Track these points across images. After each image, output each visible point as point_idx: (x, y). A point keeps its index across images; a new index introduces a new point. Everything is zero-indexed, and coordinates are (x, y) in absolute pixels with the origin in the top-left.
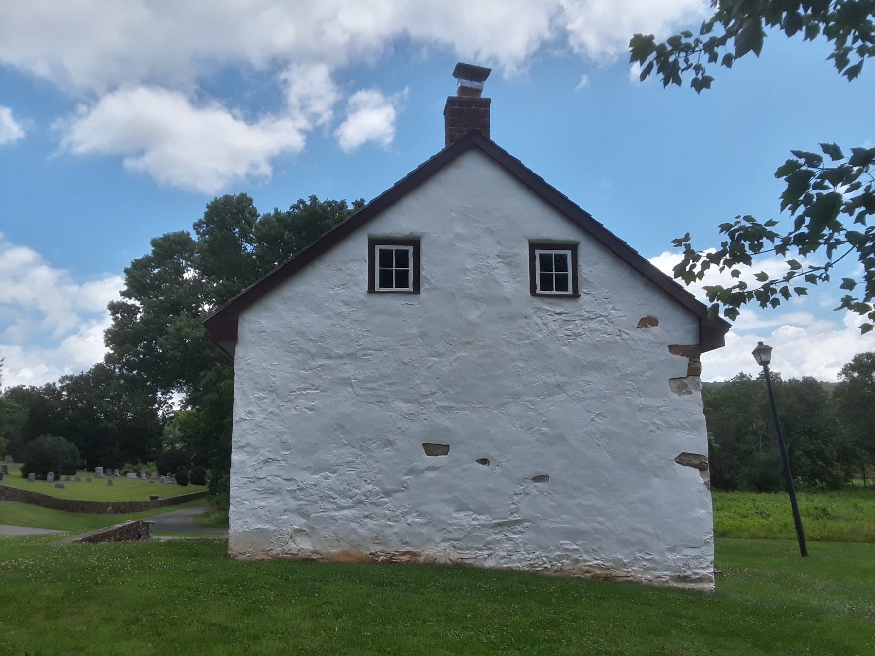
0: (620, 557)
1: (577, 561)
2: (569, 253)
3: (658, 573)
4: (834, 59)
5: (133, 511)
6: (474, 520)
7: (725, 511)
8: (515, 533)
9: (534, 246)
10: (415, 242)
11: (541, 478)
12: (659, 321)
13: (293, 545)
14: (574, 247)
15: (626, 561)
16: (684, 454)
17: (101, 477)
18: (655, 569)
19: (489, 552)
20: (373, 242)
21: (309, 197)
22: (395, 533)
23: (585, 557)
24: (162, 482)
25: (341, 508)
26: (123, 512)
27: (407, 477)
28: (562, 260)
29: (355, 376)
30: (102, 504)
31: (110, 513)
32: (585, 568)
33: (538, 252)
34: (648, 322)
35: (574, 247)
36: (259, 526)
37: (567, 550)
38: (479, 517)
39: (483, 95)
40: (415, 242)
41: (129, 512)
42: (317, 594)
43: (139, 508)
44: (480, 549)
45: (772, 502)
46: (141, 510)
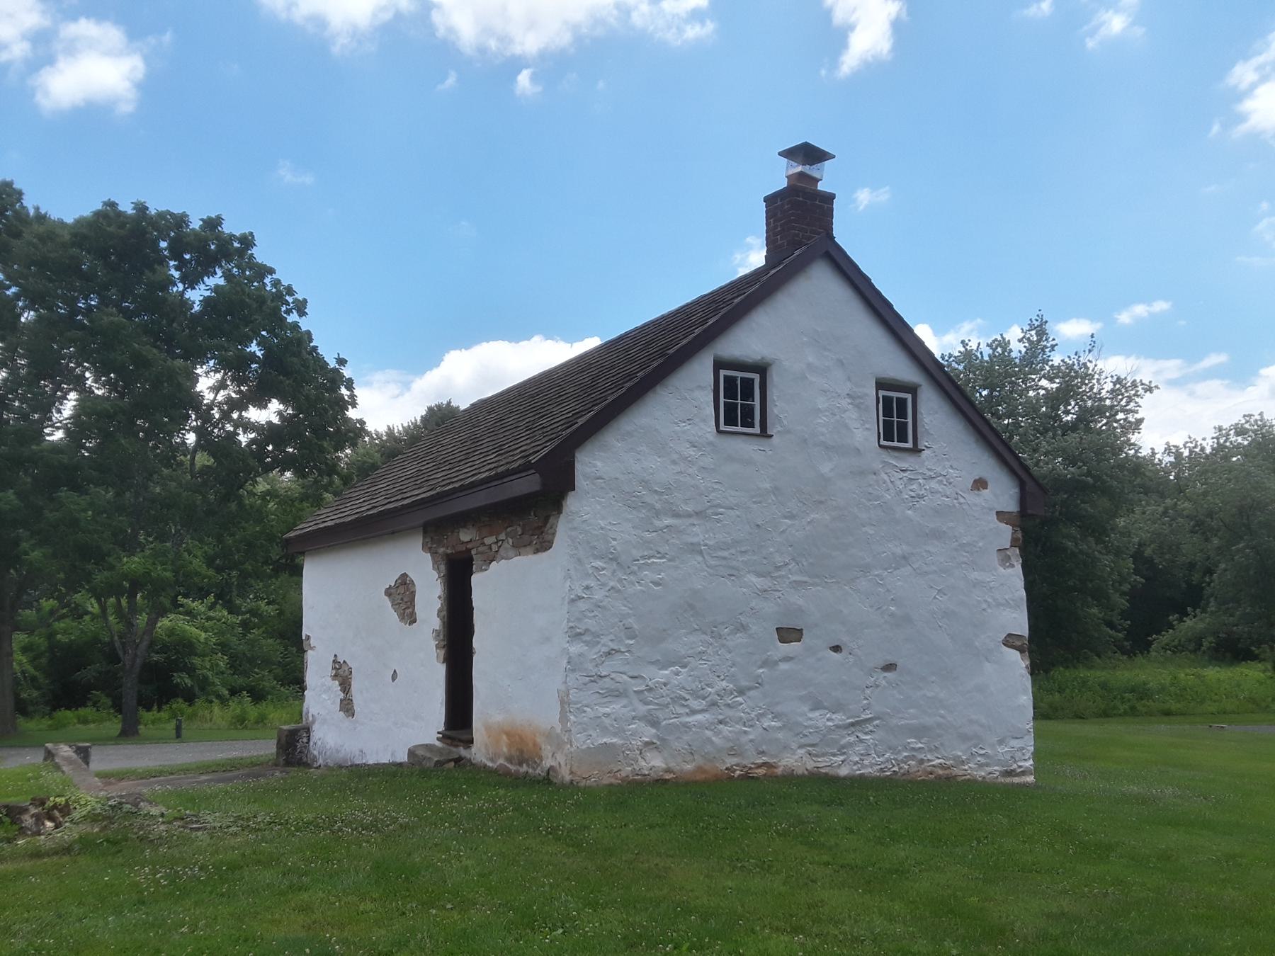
0: (960, 754)
1: (921, 762)
2: (757, 377)
3: (989, 769)
8: (866, 734)
9: (881, 385)
11: (890, 667)
12: (989, 483)
16: (1010, 635)
18: (987, 765)
19: (842, 758)
20: (719, 365)
22: (751, 741)
23: (929, 757)
25: (694, 712)
27: (761, 671)
28: (748, 384)
32: (929, 769)
33: (722, 373)
34: (980, 484)
35: (913, 389)
36: (605, 740)
37: (913, 749)
38: (834, 717)
40: (762, 369)
44: (834, 755)
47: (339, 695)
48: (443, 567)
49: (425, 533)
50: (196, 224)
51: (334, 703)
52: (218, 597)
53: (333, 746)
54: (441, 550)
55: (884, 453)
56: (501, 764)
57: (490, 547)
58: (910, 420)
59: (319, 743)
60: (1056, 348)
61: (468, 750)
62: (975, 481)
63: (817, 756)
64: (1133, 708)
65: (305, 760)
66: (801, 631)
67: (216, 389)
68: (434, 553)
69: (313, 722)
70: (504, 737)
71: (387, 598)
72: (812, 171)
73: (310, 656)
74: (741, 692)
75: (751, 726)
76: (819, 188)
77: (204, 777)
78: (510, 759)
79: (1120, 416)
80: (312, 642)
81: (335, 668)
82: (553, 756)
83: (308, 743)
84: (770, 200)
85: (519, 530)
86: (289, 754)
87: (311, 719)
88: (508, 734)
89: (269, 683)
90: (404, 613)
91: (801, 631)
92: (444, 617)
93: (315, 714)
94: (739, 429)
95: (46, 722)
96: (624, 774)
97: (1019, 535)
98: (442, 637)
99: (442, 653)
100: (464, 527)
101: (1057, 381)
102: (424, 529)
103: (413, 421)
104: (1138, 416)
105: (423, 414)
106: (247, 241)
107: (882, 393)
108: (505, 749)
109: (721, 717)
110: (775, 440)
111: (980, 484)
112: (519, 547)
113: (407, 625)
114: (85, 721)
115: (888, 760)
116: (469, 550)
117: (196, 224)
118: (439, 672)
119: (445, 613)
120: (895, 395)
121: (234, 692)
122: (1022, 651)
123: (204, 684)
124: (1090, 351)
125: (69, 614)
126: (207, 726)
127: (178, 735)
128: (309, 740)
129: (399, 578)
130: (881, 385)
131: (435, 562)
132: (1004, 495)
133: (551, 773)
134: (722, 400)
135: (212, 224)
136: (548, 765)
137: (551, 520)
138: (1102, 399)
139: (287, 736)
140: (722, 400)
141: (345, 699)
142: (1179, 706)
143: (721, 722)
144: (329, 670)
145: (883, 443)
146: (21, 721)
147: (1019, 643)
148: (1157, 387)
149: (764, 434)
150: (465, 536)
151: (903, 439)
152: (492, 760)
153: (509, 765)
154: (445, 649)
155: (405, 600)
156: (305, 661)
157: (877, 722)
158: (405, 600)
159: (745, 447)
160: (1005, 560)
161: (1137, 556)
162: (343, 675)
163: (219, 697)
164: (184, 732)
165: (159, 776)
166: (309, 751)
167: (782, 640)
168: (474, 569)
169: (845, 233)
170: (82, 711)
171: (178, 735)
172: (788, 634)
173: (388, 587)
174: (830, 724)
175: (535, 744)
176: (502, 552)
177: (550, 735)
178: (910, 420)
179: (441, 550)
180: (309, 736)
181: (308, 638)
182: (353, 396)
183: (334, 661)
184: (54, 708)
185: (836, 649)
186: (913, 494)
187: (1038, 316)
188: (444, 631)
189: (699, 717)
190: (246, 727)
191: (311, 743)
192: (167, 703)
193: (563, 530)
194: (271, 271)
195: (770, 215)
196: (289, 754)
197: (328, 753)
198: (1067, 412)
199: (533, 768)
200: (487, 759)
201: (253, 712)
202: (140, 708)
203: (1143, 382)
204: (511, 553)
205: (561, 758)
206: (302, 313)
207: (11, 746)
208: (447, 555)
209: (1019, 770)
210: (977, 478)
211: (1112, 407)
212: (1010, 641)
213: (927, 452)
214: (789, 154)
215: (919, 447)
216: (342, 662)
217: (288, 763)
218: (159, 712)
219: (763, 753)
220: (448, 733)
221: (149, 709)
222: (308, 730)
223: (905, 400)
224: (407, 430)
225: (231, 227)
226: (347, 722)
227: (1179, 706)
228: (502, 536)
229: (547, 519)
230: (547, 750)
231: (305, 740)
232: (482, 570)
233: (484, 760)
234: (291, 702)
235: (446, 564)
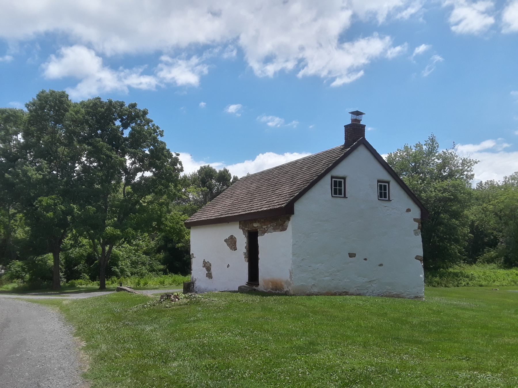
0: (401, 291)
1: (390, 293)
2: (343, 180)
3: (410, 296)
6: (363, 280)
8: (374, 284)
9: (379, 181)
10: (344, 178)
11: (381, 265)
12: (411, 209)
13: (312, 290)
14: (388, 182)
15: (403, 292)
16: (417, 256)
18: (410, 294)
19: (367, 291)
20: (332, 177)
21: (419, 142)
22: (341, 285)
23: (392, 291)
25: (326, 276)
27: (344, 265)
28: (340, 183)
32: (392, 295)
33: (333, 180)
34: (408, 210)
35: (388, 182)
36: (302, 283)
37: (388, 289)
38: (365, 279)
39: (361, 123)
40: (344, 178)
42: (202, 104)
44: (365, 290)
48: (247, 234)
50: (127, 105)
52: (125, 239)
54: (246, 229)
55: (379, 201)
56: (269, 291)
57: (265, 229)
58: (387, 191)
59: (198, 287)
60: (439, 146)
61: (257, 287)
62: (407, 209)
63: (360, 290)
64: (468, 284)
66: (355, 254)
67: (132, 164)
68: (243, 230)
70: (270, 283)
71: (225, 242)
72: (358, 117)
73: (194, 261)
74: (338, 271)
75: (341, 281)
76: (361, 123)
78: (272, 289)
79: (465, 173)
82: (287, 287)
83: (193, 287)
84: (346, 127)
85: (275, 224)
87: (194, 280)
88: (272, 282)
91: (355, 254)
93: (196, 278)
94: (338, 196)
96: (307, 293)
97: (421, 226)
98: (247, 254)
99: (247, 259)
100: (255, 222)
101: (441, 159)
103: (194, 172)
104: (472, 173)
105: (199, 170)
106: (145, 113)
107: (379, 184)
108: (271, 287)
109: (333, 278)
110: (348, 198)
111: (408, 210)
112: (275, 229)
115: (380, 292)
116: (257, 229)
117: (127, 105)
118: (245, 265)
119: (247, 247)
120: (383, 184)
121: (132, 274)
122: (421, 261)
123: (122, 271)
124: (453, 148)
130: (379, 181)
131: (244, 232)
132: (416, 212)
133: (287, 292)
134: (333, 187)
135: (133, 106)
136: (286, 290)
137: (286, 222)
138: (458, 167)
140: (333, 187)
141: (208, 273)
142: (485, 283)
143: (333, 280)
144: (202, 264)
145: (379, 198)
147: (420, 258)
148: (479, 161)
149: (345, 197)
150: (255, 225)
151: (385, 197)
152: (266, 290)
153: (272, 291)
155: (232, 243)
157: (377, 281)
158: (232, 243)
159: (340, 201)
160: (416, 234)
161: (472, 226)
162: (207, 266)
163: (128, 276)
166: (194, 290)
167: (350, 257)
168: (259, 234)
169: (369, 136)
172: (352, 255)
174: (364, 281)
175: (281, 285)
176: (269, 230)
177: (287, 282)
178: (387, 191)
179: (246, 229)
181: (193, 254)
182: (182, 168)
185: (365, 259)
186: (388, 214)
187: (432, 135)
189: (327, 278)
191: (195, 287)
192: (110, 278)
193: (290, 225)
194: (152, 121)
195: (346, 131)
197: (202, 290)
198: (445, 172)
199: (281, 291)
200: (264, 290)
203: (474, 160)
204: (272, 231)
205: (290, 288)
206: (162, 136)
208: (248, 230)
209: (419, 296)
210: (408, 208)
211: (462, 170)
212: (417, 258)
213: (393, 201)
214: (353, 113)
215: (390, 200)
219: (344, 288)
220: (250, 282)
223: (386, 185)
224: (191, 176)
225: (140, 107)
227: (485, 283)
228: (269, 226)
229: (285, 222)
230: (285, 286)
231: (192, 286)
232: (262, 235)
233: (263, 290)
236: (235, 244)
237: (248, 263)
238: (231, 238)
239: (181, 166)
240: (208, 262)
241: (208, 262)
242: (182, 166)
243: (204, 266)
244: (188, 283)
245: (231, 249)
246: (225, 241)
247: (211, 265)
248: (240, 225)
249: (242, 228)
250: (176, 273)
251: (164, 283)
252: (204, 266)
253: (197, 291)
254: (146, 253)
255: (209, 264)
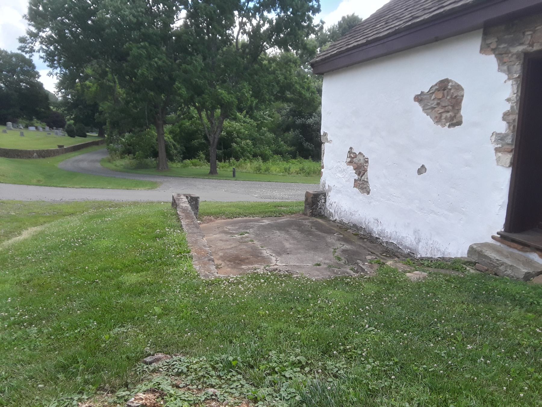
4: (244, 18)
5: (50, 156)
7: (167, 125)
17: (11, 129)
24: (57, 134)
26: (44, 157)
29: (113, 58)
30: (29, 151)
31: (36, 158)
41: (47, 157)
43: (53, 154)
45: (431, 309)
46: (54, 155)
47: (354, 176)
48: (517, 68)
49: (486, 35)
51: (348, 180)
53: (347, 210)
59: (334, 205)
65: (323, 213)
68: (500, 56)
69: (330, 190)
77: (266, 222)
80: (329, 137)
81: (350, 157)
83: (325, 202)
86: (313, 209)
87: (327, 188)
89: (268, 152)
90: (441, 117)
92: (514, 120)
93: (331, 185)
95: (179, 165)
98: (509, 140)
99: (508, 158)
102: (484, 31)
113: (446, 127)
114: (195, 165)
125: (369, 261)
126: (244, 171)
127: (234, 176)
128: (325, 201)
129: (436, 85)
139: (312, 198)
144: (345, 158)
146: (170, 164)
154: (513, 152)
156: (322, 150)
164: (236, 174)
165: (239, 217)
170: (194, 160)
171: (234, 176)
173: (419, 93)
180: (325, 199)
181: (325, 134)
182: (319, 6)
183: (349, 152)
184: (184, 158)
188: (513, 136)
190: (261, 173)
191: (327, 204)
196: (313, 209)
197: (343, 214)
201: (263, 166)
202: (217, 161)
207: (166, 176)
216: (357, 154)
217: (313, 215)
218: (224, 162)
220: (507, 234)
221: (220, 161)
222: (325, 195)
226: (361, 197)
231: (323, 201)
234: (278, 162)
235: (523, 64)
236: (453, 107)
237: (510, 169)
238: (438, 90)
239: (317, 4)
240: (360, 153)
241: (360, 153)
242: (318, 3)
243: (350, 163)
244: (314, 195)
245: (438, 120)
246: (419, 99)
247: (367, 162)
248: (484, 39)
249: (494, 51)
250: (306, 158)
251: (289, 170)
252: (350, 163)
253: (333, 212)
254: (271, 130)
255: (362, 158)
